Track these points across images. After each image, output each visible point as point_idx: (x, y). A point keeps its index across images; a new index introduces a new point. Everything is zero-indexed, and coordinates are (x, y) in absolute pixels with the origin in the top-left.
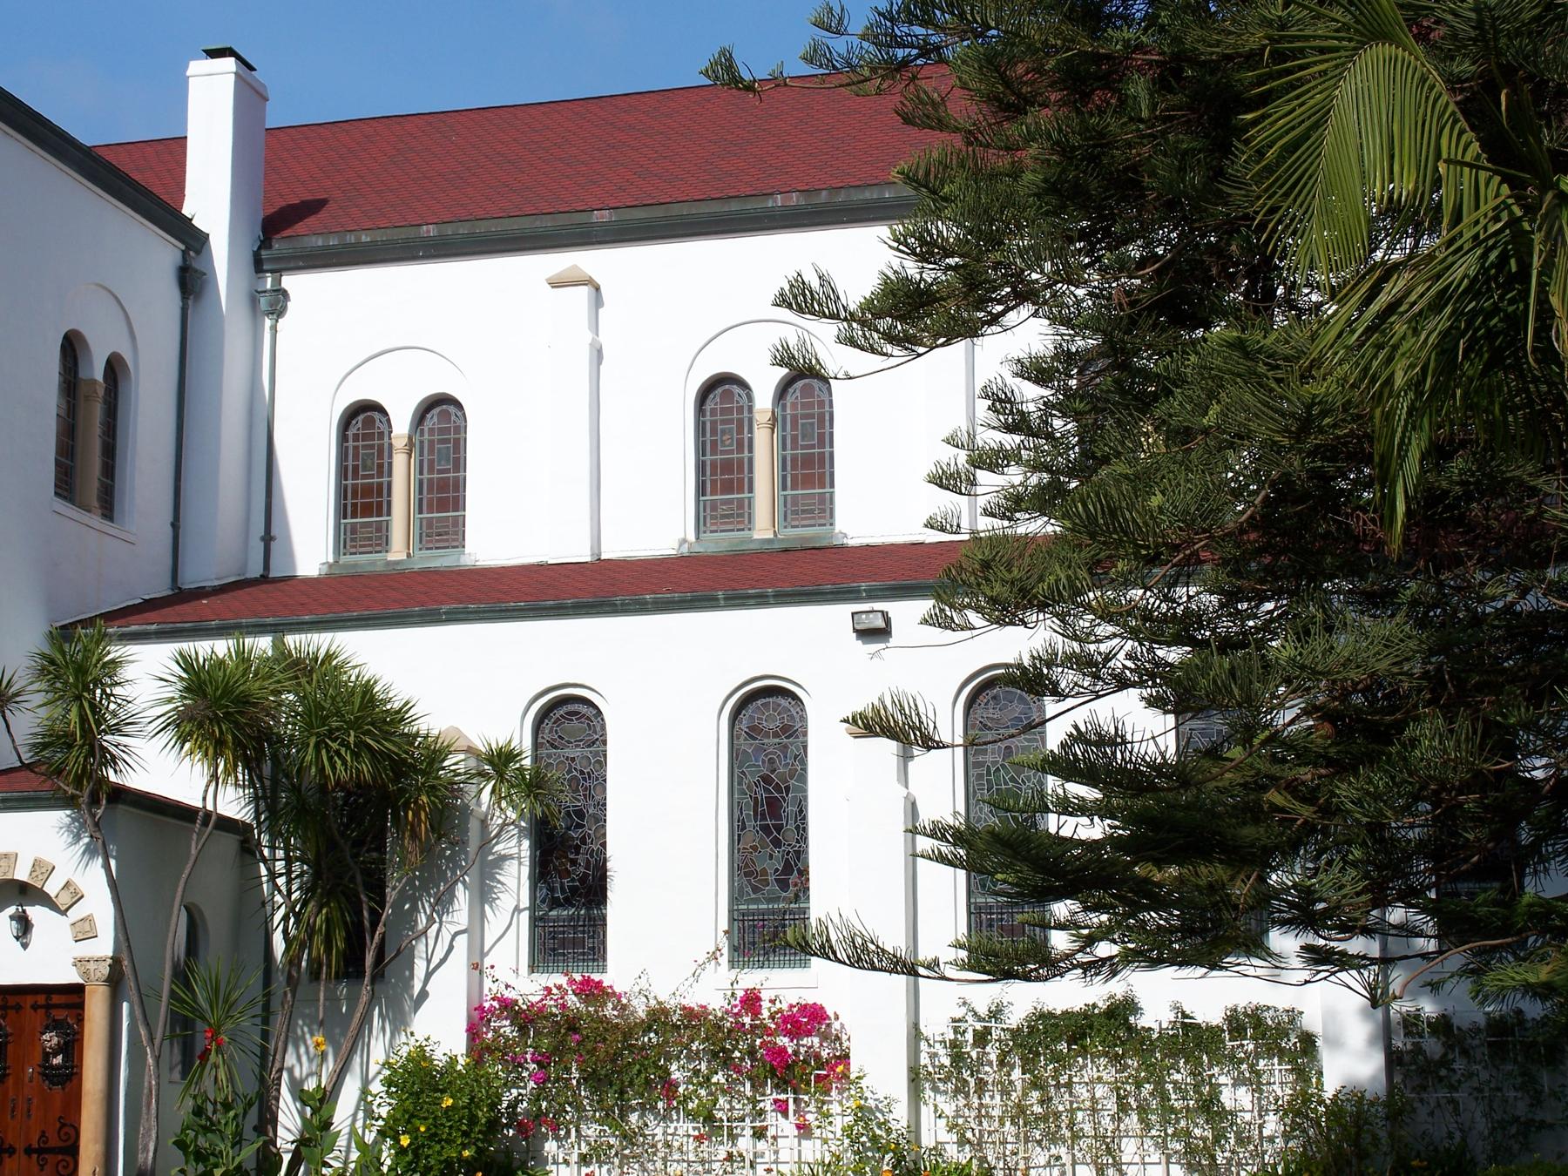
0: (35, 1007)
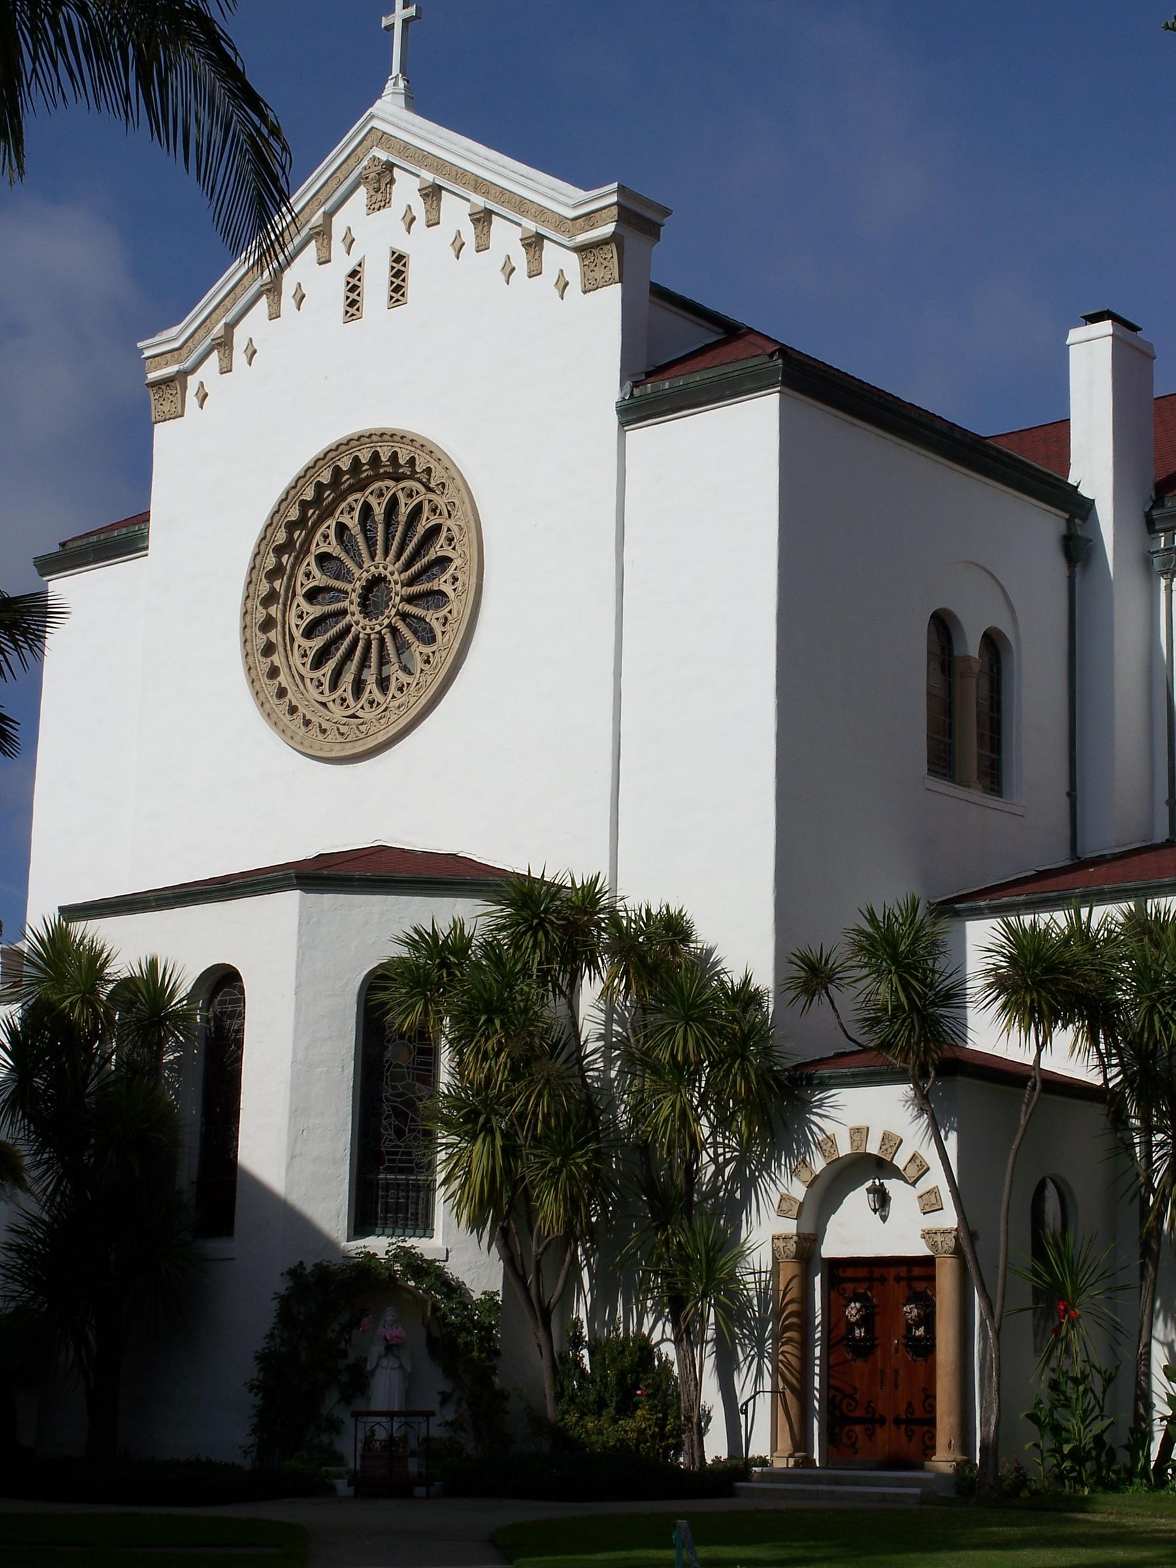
0: (898, 1279)
